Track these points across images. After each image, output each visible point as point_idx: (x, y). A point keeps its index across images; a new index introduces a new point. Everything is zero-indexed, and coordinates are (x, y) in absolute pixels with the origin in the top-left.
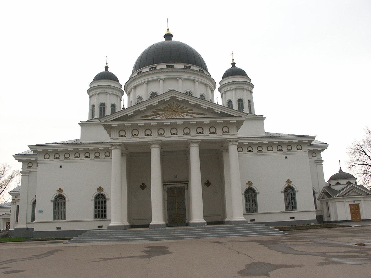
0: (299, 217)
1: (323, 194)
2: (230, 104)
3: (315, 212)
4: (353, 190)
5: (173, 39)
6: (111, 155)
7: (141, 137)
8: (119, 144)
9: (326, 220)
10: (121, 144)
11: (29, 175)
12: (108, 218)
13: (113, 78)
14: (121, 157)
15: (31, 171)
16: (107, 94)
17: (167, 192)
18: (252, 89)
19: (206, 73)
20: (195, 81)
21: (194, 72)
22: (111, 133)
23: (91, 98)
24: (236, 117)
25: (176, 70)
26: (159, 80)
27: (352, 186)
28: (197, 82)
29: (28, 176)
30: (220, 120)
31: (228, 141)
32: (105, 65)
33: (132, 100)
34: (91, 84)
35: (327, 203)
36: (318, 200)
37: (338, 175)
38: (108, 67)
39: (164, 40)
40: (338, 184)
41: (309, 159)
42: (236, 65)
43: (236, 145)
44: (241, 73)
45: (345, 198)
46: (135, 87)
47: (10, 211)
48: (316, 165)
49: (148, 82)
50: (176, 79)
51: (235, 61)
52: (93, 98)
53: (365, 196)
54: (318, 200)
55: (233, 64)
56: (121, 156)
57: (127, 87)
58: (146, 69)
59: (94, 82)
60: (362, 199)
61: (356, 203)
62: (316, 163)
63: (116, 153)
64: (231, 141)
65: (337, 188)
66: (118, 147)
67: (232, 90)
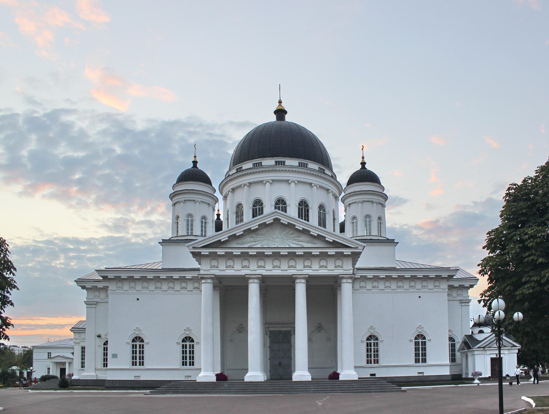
0: (429, 372)
1: (463, 344)
2: (355, 221)
3: (449, 366)
6: (201, 286)
9: (464, 376)
10: (213, 277)
11: (95, 308)
12: (196, 366)
13: (206, 180)
14: (213, 291)
15: (99, 301)
16: (196, 202)
17: (269, 337)
19: (330, 174)
20: (313, 185)
21: (312, 173)
22: (201, 262)
23: (175, 206)
24: (352, 248)
25: (287, 169)
28: (315, 187)
29: (94, 309)
31: (341, 277)
33: (228, 206)
34: (175, 186)
35: (467, 355)
38: (197, 162)
40: (481, 332)
42: (366, 166)
43: (350, 283)
44: (372, 178)
46: (233, 190)
47: (73, 353)
48: (461, 306)
49: (250, 183)
52: (177, 205)
53: (510, 348)
56: (213, 290)
58: (248, 165)
62: (461, 303)
63: (207, 288)
65: (479, 337)
66: (209, 281)
67: (358, 203)
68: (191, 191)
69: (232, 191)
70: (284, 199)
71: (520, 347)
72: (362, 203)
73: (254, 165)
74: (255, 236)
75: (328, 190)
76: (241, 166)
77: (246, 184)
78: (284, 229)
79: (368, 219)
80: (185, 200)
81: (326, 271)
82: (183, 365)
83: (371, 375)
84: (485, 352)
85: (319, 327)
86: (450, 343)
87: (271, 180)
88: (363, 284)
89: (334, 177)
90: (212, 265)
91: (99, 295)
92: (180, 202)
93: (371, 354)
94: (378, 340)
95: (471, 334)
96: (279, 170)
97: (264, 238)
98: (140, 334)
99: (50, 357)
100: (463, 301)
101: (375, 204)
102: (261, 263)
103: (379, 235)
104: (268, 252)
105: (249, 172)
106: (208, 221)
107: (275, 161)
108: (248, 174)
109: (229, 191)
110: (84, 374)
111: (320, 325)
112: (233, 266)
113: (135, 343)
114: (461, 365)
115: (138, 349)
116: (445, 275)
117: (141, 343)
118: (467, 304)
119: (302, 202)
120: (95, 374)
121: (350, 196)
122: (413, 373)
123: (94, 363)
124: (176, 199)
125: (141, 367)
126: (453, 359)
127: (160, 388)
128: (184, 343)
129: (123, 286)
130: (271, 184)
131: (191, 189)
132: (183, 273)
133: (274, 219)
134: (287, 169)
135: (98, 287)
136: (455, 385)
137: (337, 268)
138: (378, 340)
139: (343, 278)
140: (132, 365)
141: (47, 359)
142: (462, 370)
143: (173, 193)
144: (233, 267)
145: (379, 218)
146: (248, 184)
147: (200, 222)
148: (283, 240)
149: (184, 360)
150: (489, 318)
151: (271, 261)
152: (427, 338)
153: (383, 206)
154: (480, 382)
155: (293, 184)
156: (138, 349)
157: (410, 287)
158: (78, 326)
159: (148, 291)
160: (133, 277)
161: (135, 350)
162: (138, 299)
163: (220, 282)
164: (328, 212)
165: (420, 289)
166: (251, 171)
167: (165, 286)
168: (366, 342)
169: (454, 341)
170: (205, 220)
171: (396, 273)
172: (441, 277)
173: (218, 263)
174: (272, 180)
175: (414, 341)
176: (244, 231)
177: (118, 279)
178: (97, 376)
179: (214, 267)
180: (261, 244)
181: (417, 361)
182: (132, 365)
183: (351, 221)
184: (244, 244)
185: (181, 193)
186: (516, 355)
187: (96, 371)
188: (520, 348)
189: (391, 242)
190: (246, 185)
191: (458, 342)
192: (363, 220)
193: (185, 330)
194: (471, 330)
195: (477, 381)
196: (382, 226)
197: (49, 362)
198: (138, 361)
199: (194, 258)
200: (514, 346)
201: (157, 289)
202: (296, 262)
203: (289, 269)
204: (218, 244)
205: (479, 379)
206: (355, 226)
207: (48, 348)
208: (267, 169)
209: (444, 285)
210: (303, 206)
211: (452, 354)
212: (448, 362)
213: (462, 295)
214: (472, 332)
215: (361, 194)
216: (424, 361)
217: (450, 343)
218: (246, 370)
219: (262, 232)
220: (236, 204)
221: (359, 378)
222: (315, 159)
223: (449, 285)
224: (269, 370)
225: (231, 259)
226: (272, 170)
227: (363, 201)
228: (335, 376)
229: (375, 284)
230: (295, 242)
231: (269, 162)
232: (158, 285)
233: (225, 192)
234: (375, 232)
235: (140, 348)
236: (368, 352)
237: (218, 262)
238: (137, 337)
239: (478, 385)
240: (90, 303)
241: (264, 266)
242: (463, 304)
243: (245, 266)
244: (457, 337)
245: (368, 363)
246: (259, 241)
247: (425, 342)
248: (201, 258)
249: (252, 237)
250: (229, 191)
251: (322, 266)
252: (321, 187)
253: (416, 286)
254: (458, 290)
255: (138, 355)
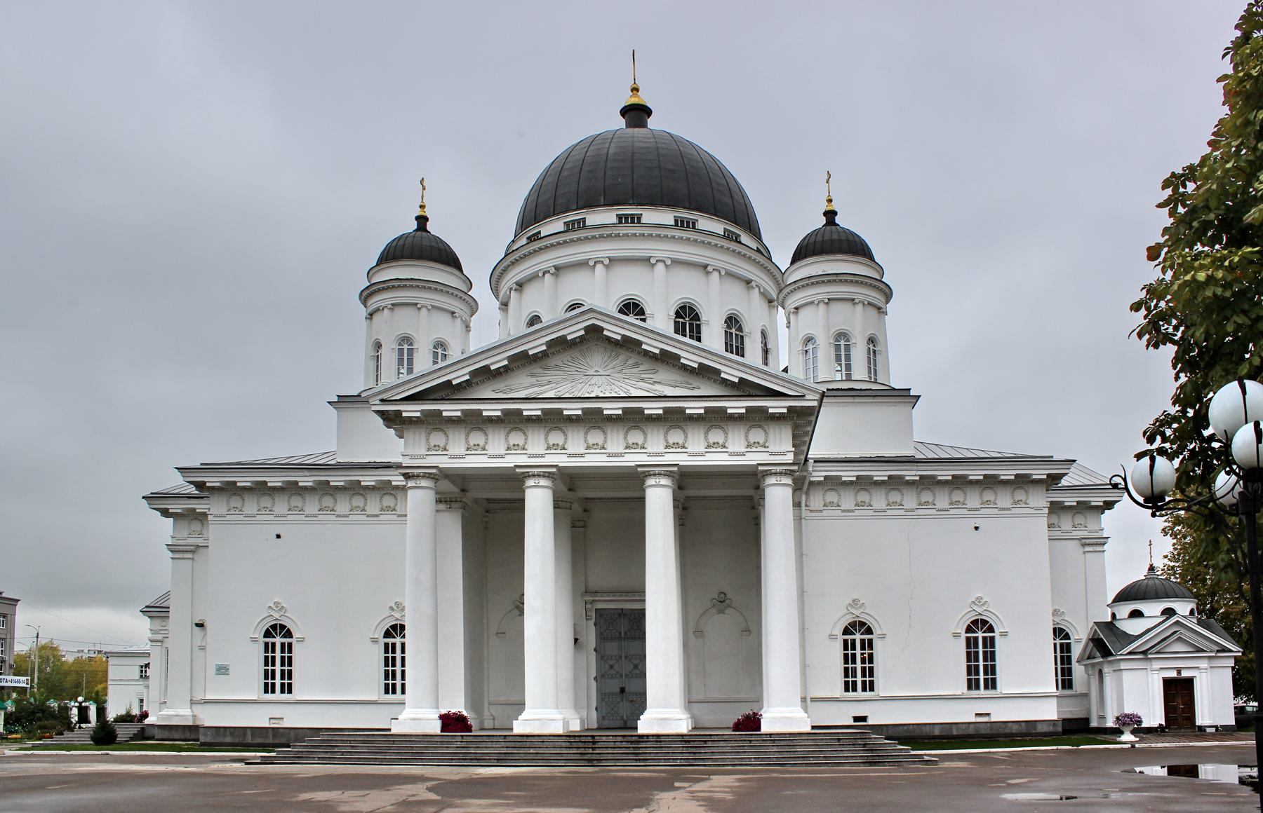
0: (1003, 712)
1: (1091, 645)
2: (810, 347)
3: (1054, 701)
4: (1175, 637)
5: (652, 123)
7: (574, 452)
8: (429, 473)
10: (435, 474)
11: (193, 559)
13: (449, 259)
16: (419, 309)
17: (595, 624)
18: (887, 302)
19: (754, 245)
20: (709, 269)
23: (371, 319)
25: (647, 231)
26: (591, 263)
27: (1177, 623)
28: (716, 274)
29: (190, 561)
30: (736, 406)
31: (763, 471)
32: (418, 212)
34: (371, 273)
35: (1101, 672)
36: (1077, 662)
37: (1140, 585)
38: (426, 219)
39: (621, 123)
40: (1136, 614)
41: (1049, 536)
44: (856, 247)
45: (1149, 659)
46: (520, 285)
48: (1085, 552)
49: (557, 268)
50: (646, 261)
51: (834, 206)
52: (377, 317)
53: (1214, 655)
54: (1077, 662)
55: (830, 215)
57: (498, 282)
59: (378, 268)
60: (1204, 664)
61: (1185, 674)
62: (1084, 545)
63: (420, 500)
64: (770, 473)
68: (408, 283)
69: (517, 287)
70: (639, 301)
71: (1239, 651)
72: (827, 304)
73: (568, 225)
74: (540, 371)
75: (748, 282)
76: (537, 231)
77: (549, 269)
78: (613, 354)
79: (842, 343)
80: (393, 305)
81: (725, 456)
82: (387, 692)
83: (856, 719)
84: (1149, 664)
85: (720, 602)
86: (1058, 642)
87: (607, 257)
88: (832, 497)
89: (764, 252)
90: (433, 445)
91: (202, 530)
92: (383, 309)
93: (855, 668)
94: (872, 634)
95: (1109, 620)
96: (627, 235)
97: (564, 377)
98: (282, 618)
99: (144, 674)
100: (1088, 541)
101: (861, 305)
102: (556, 438)
103: (873, 380)
104: (573, 409)
105: (554, 240)
106: (451, 353)
107: (617, 215)
108: (552, 245)
109: (511, 289)
110: (165, 712)
111: (722, 595)
112: (485, 445)
113: (270, 640)
114: (1086, 696)
115: (278, 655)
116: (1039, 473)
117: (287, 640)
118: (1099, 548)
119: (683, 308)
120: (191, 713)
121: (799, 288)
122: (963, 714)
123: (189, 686)
124: (376, 301)
125: (286, 696)
126: (1066, 681)
127: (289, 747)
128: (390, 640)
129: (243, 505)
130: (607, 267)
131: (409, 277)
132: (383, 473)
133: (586, 328)
134: (647, 231)
135: (197, 511)
136: (1070, 747)
137: (754, 449)
138: (872, 634)
139: (768, 472)
140: (385, 693)
141: (137, 680)
142: (1089, 710)
143: (367, 287)
144: (484, 449)
145: (872, 340)
146: (553, 270)
147: (431, 355)
148: (612, 381)
149: (268, 679)
150: (1156, 581)
151: (582, 434)
152: (998, 629)
153: (880, 310)
154: (1138, 739)
155: (660, 266)
156: (278, 655)
157: (951, 504)
158: (160, 603)
159: (302, 517)
160: (265, 483)
161: (272, 656)
162: (278, 536)
163: (463, 490)
164: (750, 334)
165: (978, 510)
166: (561, 239)
167: (343, 506)
168: (841, 638)
169: (1067, 636)
170: (445, 350)
171: (916, 468)
172: (1031, 479)
173: (447, 440)
174: (611, 259)
175: (964, 635)
176: (511, 359)
177: (230, 489)
178: (194, 716)
179: (437, 448)
180: (556, 390)
181: (972, 684)
182: (385, 693)
183: (801, 348)
184: (511, 390)
185: (384, 289)
186: (1229, 673)
187: (194, 706)
188: (1240, 654)
189: (905, 396)
190: (549, 271)
191: (1078, 641)
192: (830, 343)
193: (392, 608)
194: (1109, 610)
195: (1127, 737)
196: (879, 358)
197: (142, 687)
198: (278, 681)
199: (389, 427)
200: (1224, 650)
201: (325, 512)
202: (645, 434)
203: (628, 451)
204: (447, 391)
205: (1134, 732)
206: (812, 359)
207: (141, 655)
208: (596, 233)
209: (1040, 500)
210: (687, 319)
211: (1062, 657)
212: (1052, 688)
213: (1086, 527)
214: (1114, 616)
215: (823, 282)
216: (991, 684)
217: (1058, 642)
218: (520, 706)
219: (556, 361)
220: (527, 317)
221: (813, 727)
222: (715, 211)
223: (1052, 503)
224: (594, 705)
225: (480, 429)
226: (609, 236)
227: (829, 299)
228: (751, 723)
229: (863, 496)
230: (641, 384)
231: (603, 217)
232: (328, 502)
233: (503, 290)
234: (860, 371)
235: (283, 651)
236: (846, 662)
237: (448, 437)
238: (276, 624)
239: (1133, 746)
240: (181, 548)
241: (564, 445)
242: (1088, 549)
243: (514, 445)
244: (1073, 626)
245: (847, 690)
246: (549, 382)
247: (992, 639)
248: (404, 426)
249: (532, 375)
250: (511, 289)
251: (714, 443)
252: (729, 274)
253: (966, 502)
254: (1074, 515)
255: (278, 668)
